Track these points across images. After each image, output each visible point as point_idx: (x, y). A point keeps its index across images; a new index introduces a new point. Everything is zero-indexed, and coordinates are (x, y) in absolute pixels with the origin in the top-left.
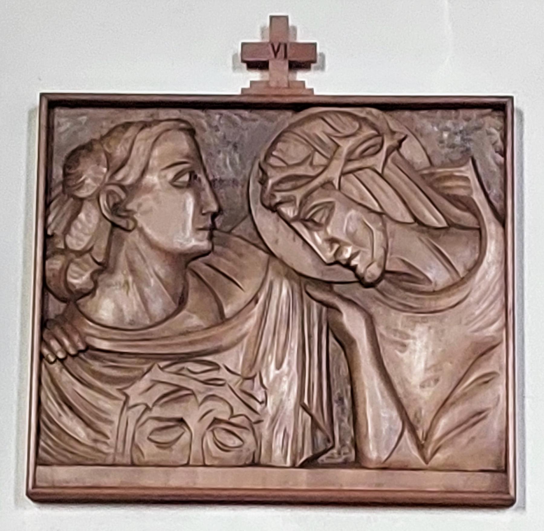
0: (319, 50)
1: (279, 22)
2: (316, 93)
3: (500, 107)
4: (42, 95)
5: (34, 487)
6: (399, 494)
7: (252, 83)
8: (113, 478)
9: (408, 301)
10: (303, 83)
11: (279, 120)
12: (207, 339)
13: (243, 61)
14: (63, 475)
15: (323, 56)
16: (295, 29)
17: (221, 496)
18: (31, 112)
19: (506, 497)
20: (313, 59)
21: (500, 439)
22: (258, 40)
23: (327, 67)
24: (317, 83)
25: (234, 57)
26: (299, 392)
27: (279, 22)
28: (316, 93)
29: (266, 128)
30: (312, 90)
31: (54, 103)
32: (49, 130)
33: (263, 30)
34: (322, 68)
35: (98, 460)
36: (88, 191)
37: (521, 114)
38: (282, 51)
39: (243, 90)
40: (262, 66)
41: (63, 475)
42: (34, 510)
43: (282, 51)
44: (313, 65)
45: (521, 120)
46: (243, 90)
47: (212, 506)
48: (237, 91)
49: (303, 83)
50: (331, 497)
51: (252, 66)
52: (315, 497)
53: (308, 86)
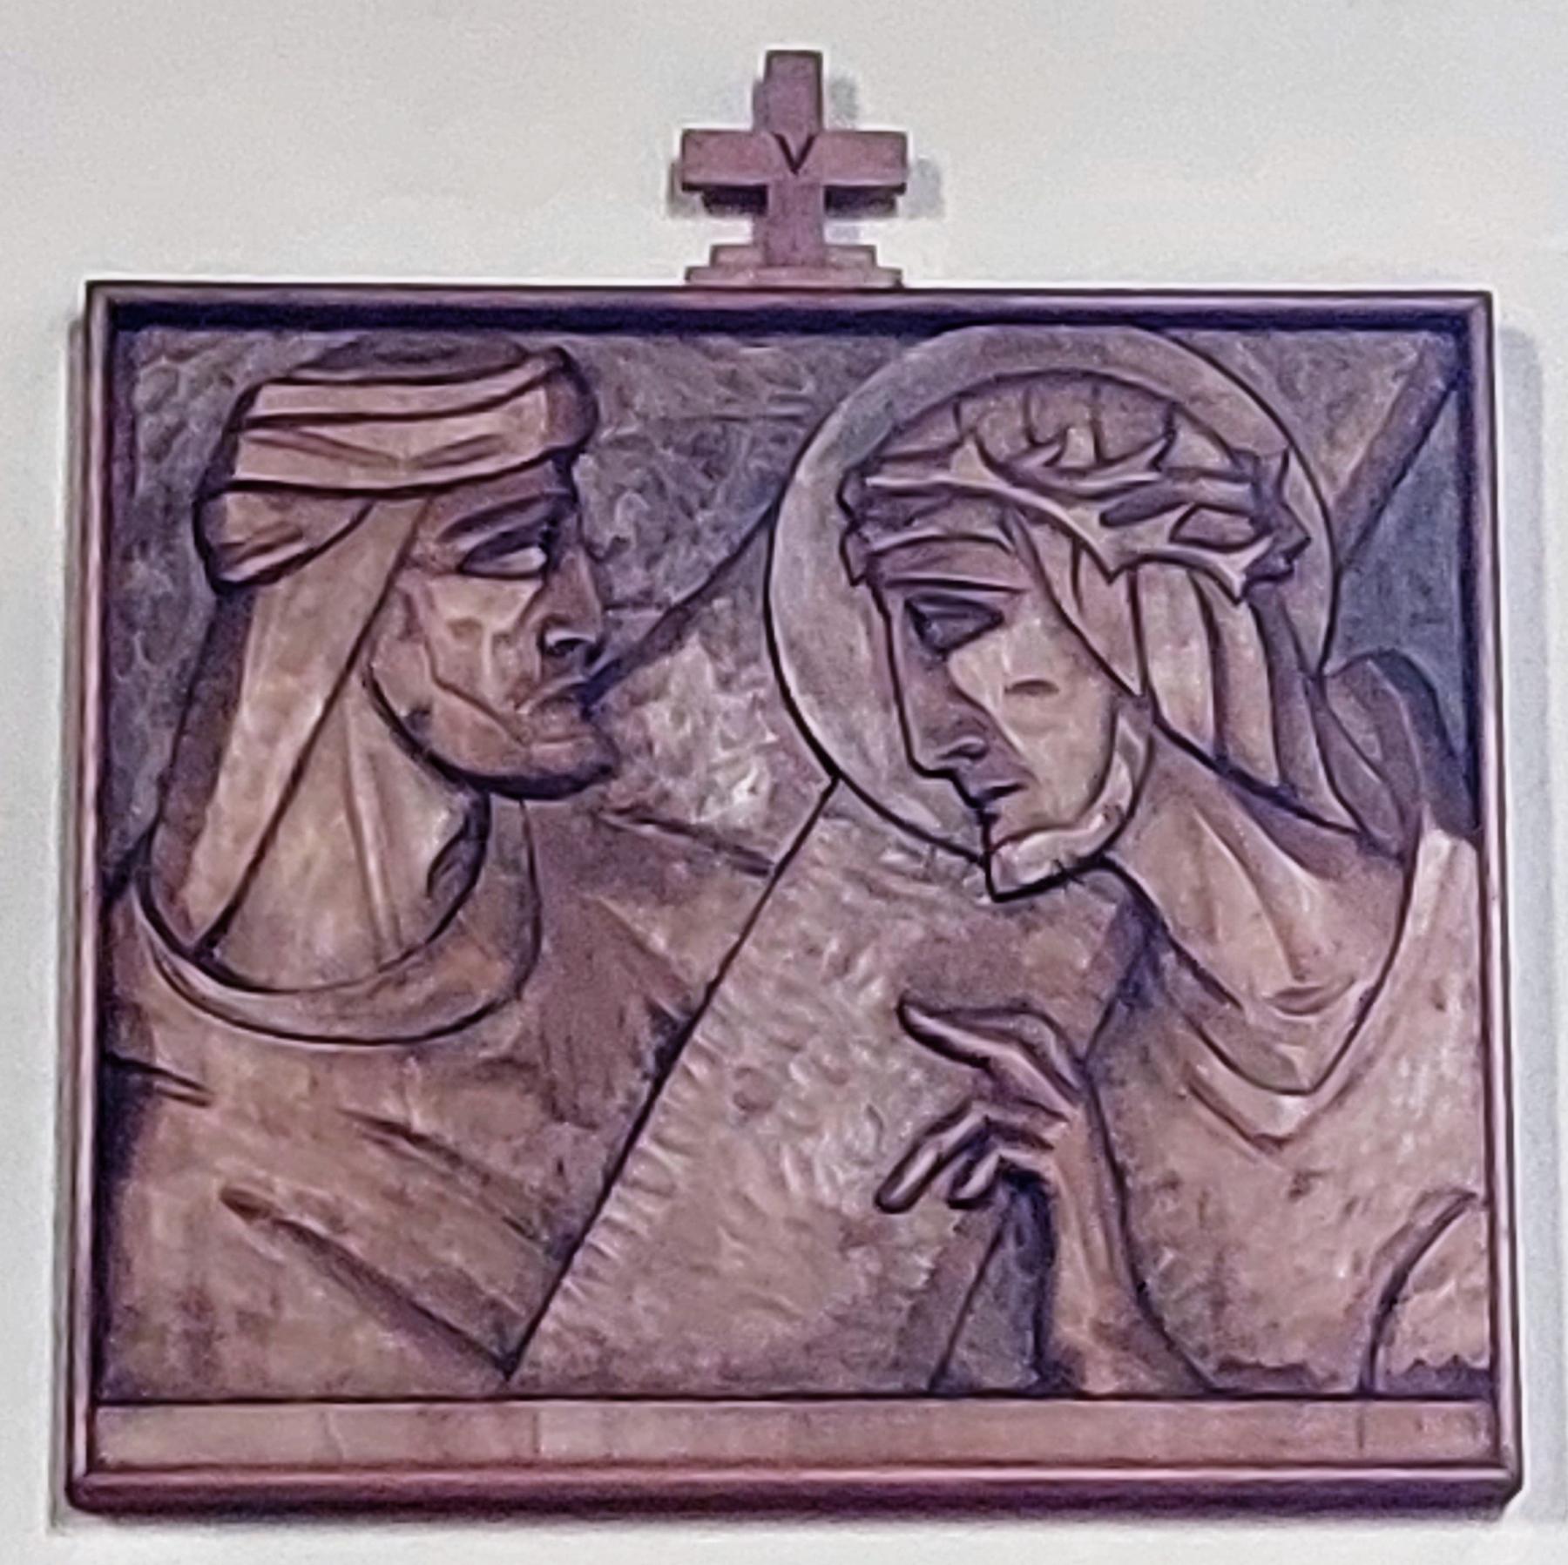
1: (794, 76)
4: (92, 287)
7: (716, 250)
10: (870, 250)
14: (137, 1440)
23: (950, 207)
24: (914, 251)
26: (402, 1515)
27: (794, 76)
28: (910, 282)
29: (777, 386)
31: (129, 320)
34: (932, 205)
36: (1209, 455)
38: (790, 158)
39: (690, 272)
40: (749, 200)
41: (137, 1440)
43: (790, 158)
44: (901, 201)
45: (1532, 378)
46: (690, 272)
48: (673, 275)
49: (870, 250)
51: (720, 199)
53: (882, 261)
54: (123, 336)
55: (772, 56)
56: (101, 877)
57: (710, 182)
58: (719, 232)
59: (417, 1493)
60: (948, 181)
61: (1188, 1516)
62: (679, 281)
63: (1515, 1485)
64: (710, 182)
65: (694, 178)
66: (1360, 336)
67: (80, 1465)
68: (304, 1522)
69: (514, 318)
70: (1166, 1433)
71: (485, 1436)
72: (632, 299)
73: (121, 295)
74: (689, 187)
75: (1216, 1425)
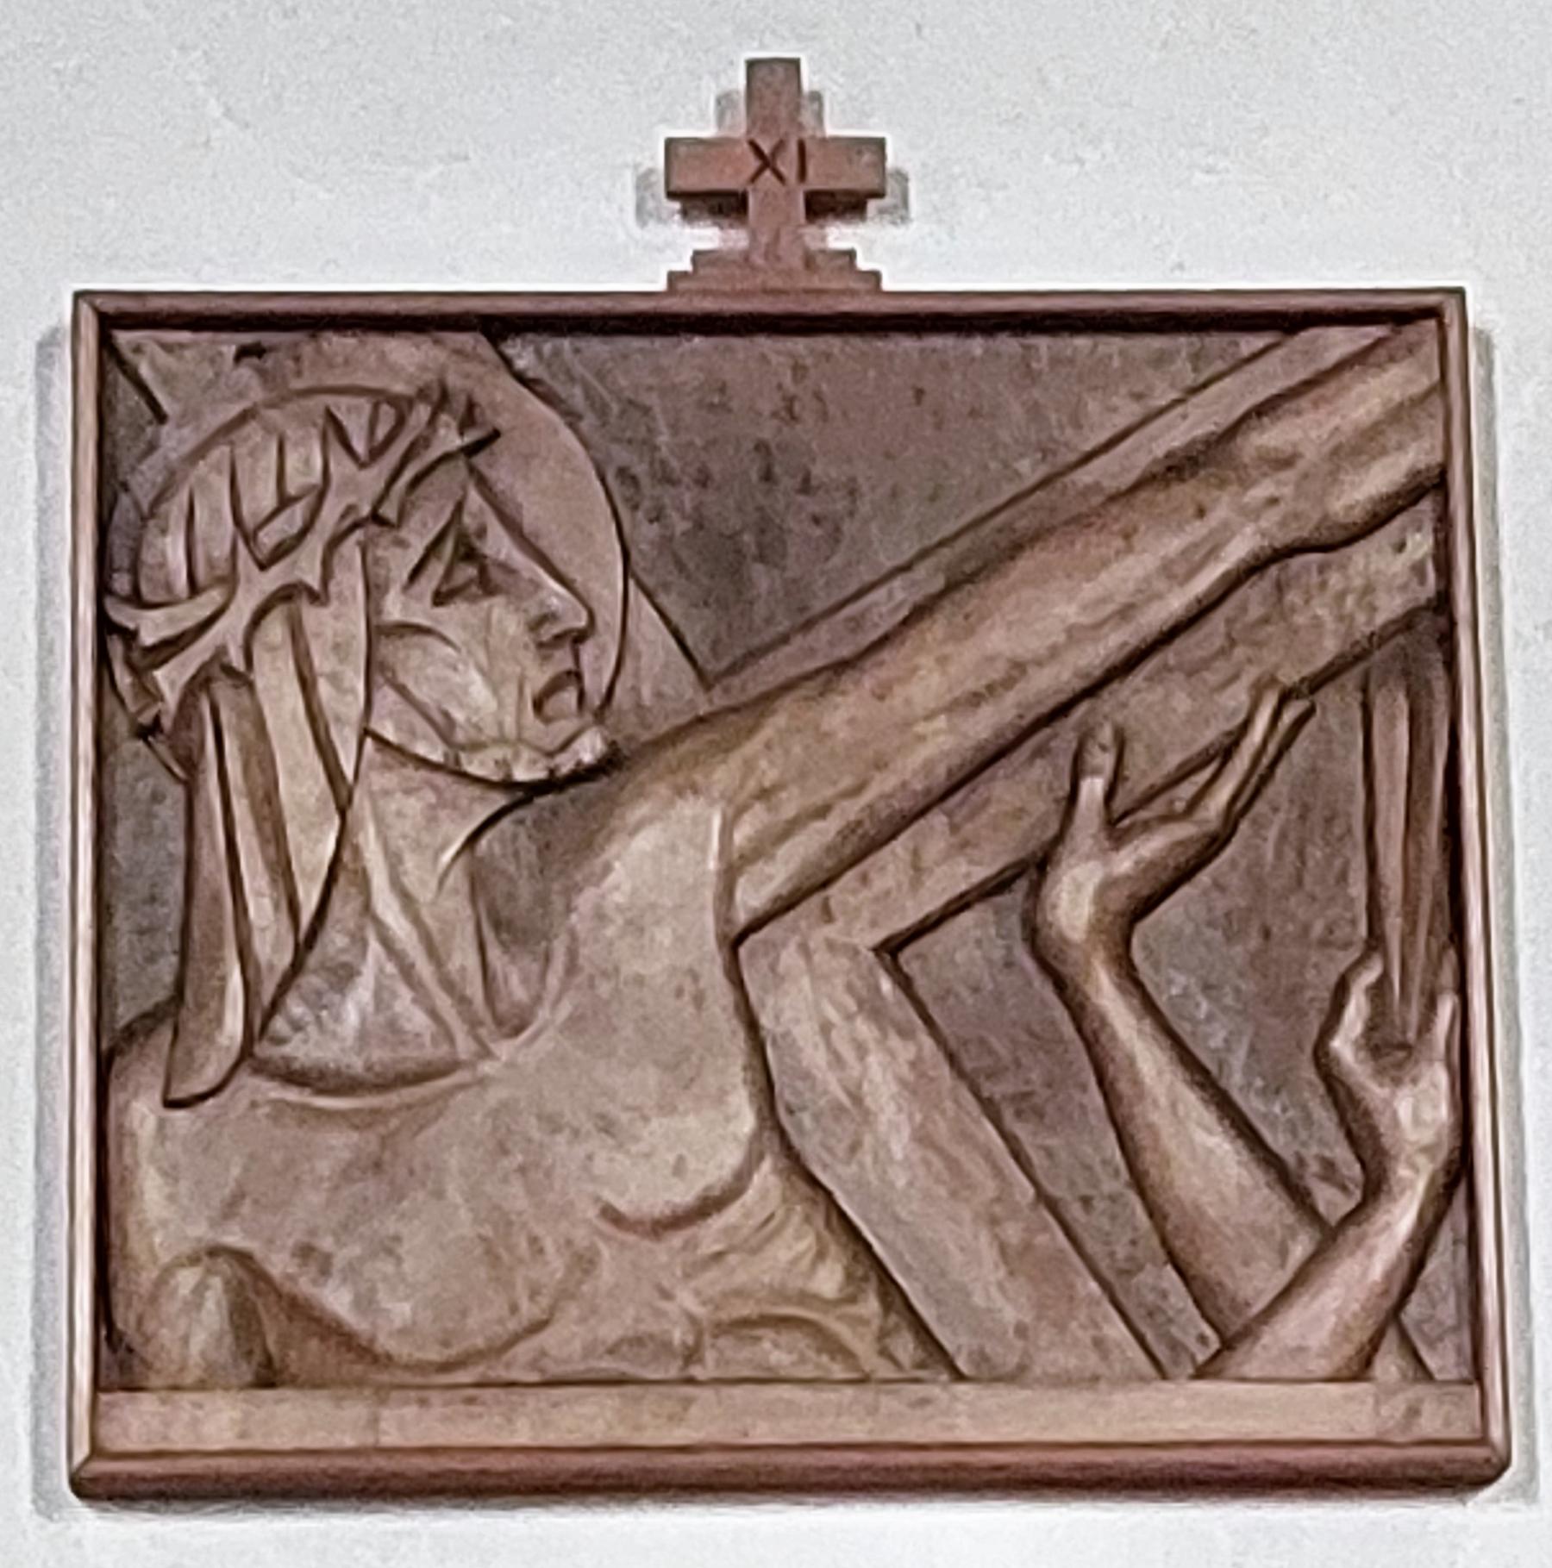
1: (773, 80)
2: (887, 285)
3: (1412, 320)
5: (96, 1451)
6: (272, 1462)
7: (697, 256)
8: (409, 1426)
10: (851, 254)
13: (672, 195)
14: (141, 1423)
15: (902, 178)
16: (816, 97)
17: (777, 1469)
18: (45, 347)
19: (1479, 1453)
22: (709, 132)
24: (901, 257)
25: (643, 183)
27: (773, 80)
28: (887, 285)
30: (875, 276)
33: (724, 102)
34: (900, 212)
37: (1487, 346)
38: (778, 165)
39: (673, 277)
40: (725, 205)
41: (141, 1423)
42: (95, 1526)
43: (778, 165)
44: (872, 205)
46: (673, 277)
47: (890, 1499)
50: (1349, 1465)
51: (702, 203)
52: (1109, 1467)
53: (863, 264)
56: (363, 881)
59: (1273, 1471)
63: (1504, 1465)
66: (1082, 342)
67: (82, 1451)
69: (794, 324)
70: (296, 1423)
72: (607, 305)
73: (109, 306)
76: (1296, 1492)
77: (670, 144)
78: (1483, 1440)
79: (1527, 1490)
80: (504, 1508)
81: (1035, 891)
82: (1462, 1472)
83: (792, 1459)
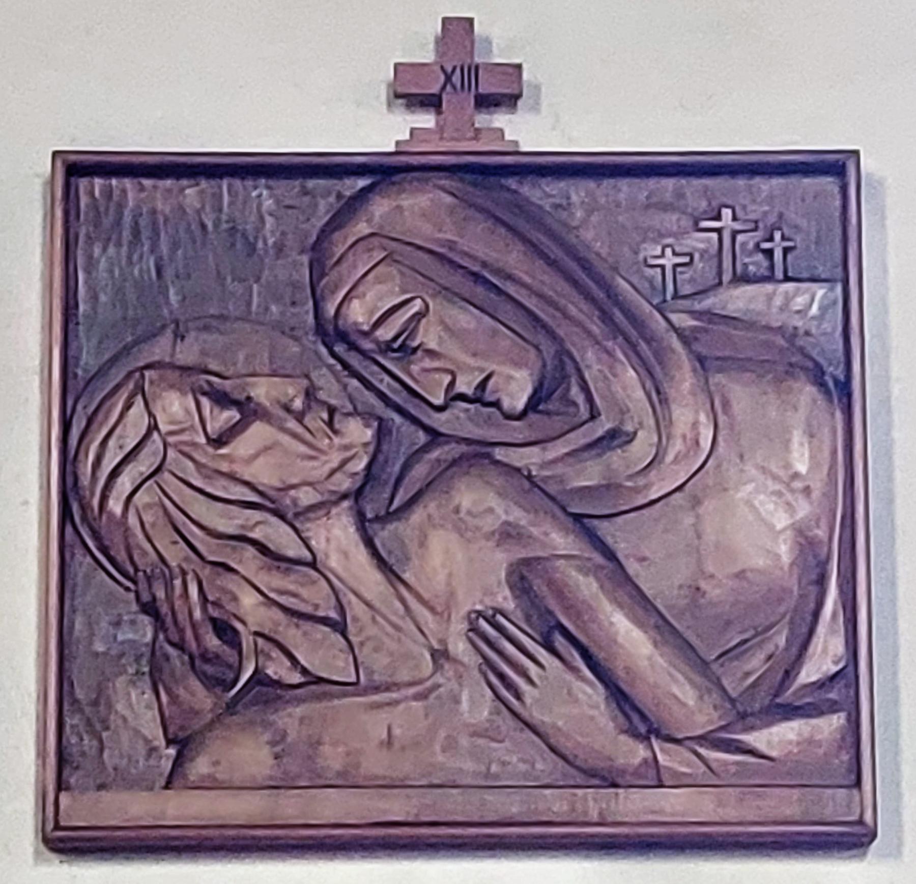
0: (525, 76)
1: (458, 30)
3: (836, 167)
5: (57, 827)
7: (413, 131)
9: (382, 307)
11: (806, 264)
12: (295, 595)
19: (856, 829)
20: (516, 92)
21: (850, 771)
24: (526, 132)
27: (458, 30)
30: (516, 143)
31: (75, 169)
32: (69, 194)
34: (535, 108)
35: (89, 564)
38: (461, 77)
39: (398, 143)
40: (431, 102)
43: (461, 77)
46: (398, 143)
48: (388, 145)
49: (501, 131)
53: (508, 137)
54: (73, 180)
55: (445, 21)
57: (410, 92)
58: (414, 122)
60: (543, 89)
61: (456, 852)
62: (392, 148)
63: (874, 836)
64: (410, 92)
65: (401, 90)
67: (50, 825)
68: (754, 855)
71: (291, 807)
73: (73, 158)
74: (398, 96)
75: (593, 802)
76: (497, 852)
77: (396, 66)
78: (861, 822)
79: (896, 851)
80: (408, 858)
81: (318, 482)
82: (854, 839)
83: (191, 833)
